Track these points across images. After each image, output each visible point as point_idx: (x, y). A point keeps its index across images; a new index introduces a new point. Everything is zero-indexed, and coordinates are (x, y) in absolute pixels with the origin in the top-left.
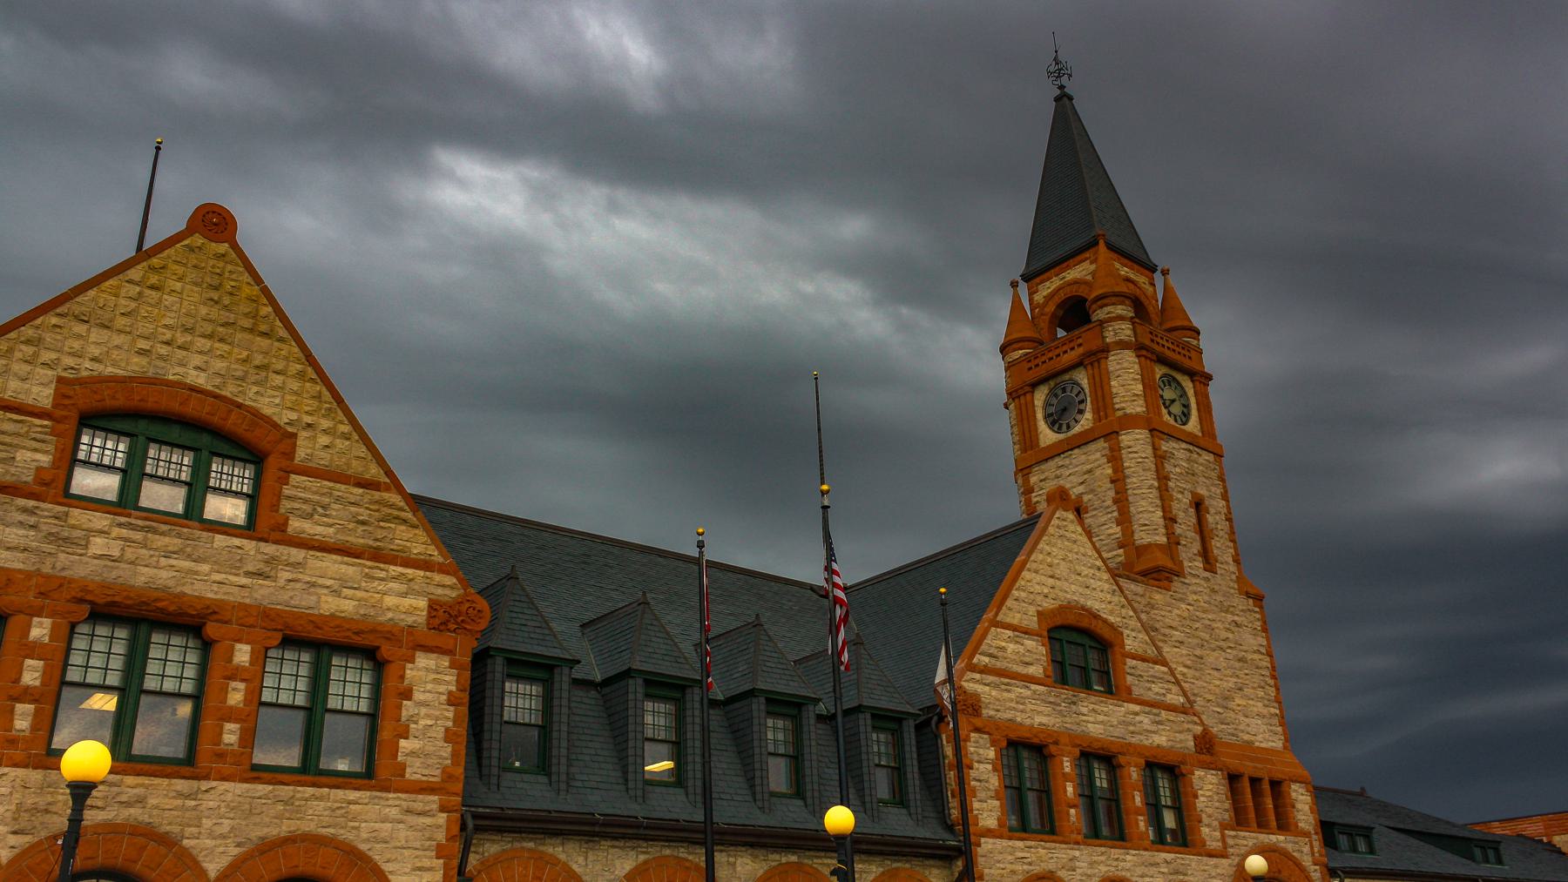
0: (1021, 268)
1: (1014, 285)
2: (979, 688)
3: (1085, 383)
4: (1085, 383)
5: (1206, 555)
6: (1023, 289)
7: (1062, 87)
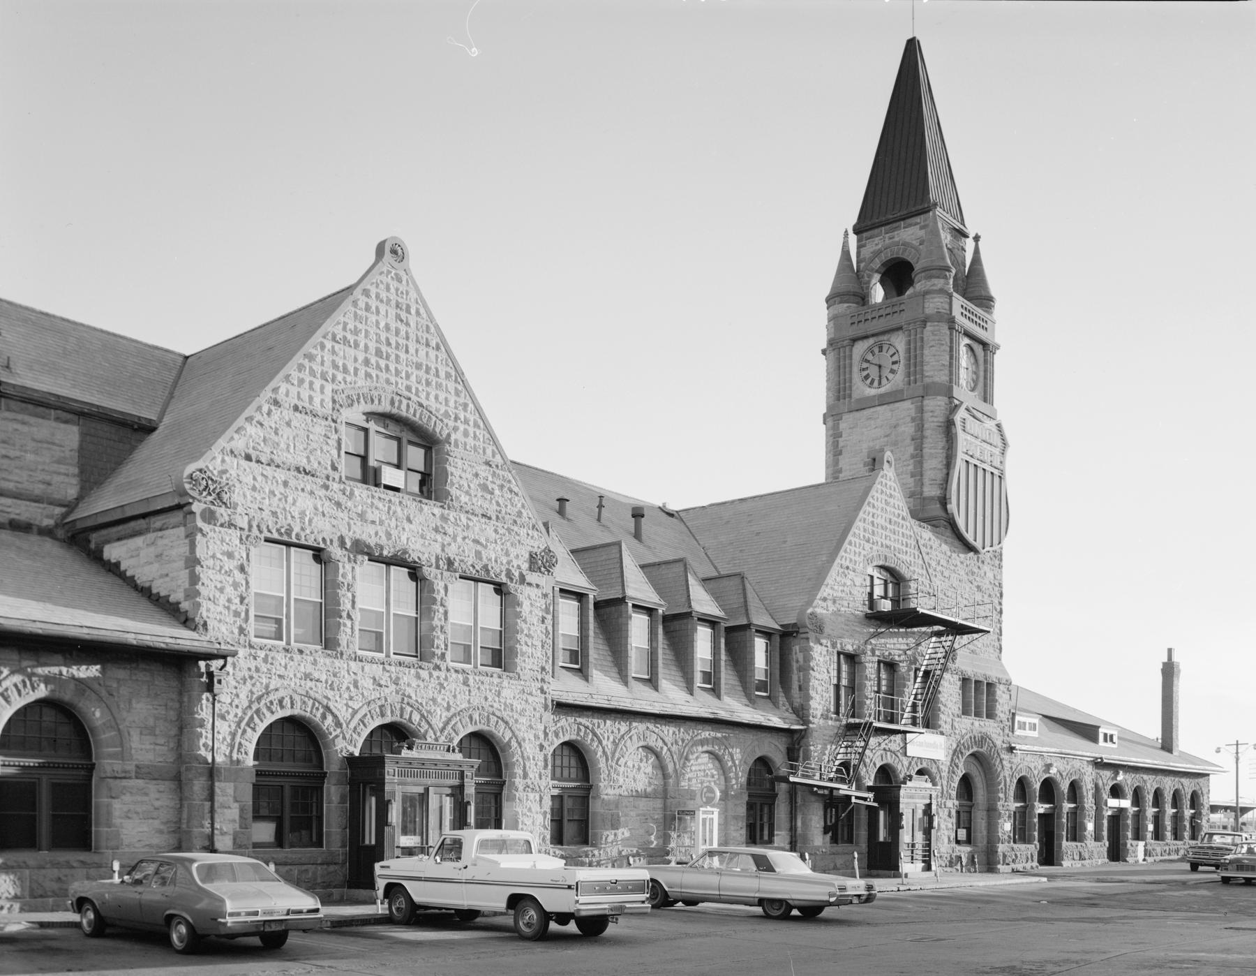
6: (853, 239)
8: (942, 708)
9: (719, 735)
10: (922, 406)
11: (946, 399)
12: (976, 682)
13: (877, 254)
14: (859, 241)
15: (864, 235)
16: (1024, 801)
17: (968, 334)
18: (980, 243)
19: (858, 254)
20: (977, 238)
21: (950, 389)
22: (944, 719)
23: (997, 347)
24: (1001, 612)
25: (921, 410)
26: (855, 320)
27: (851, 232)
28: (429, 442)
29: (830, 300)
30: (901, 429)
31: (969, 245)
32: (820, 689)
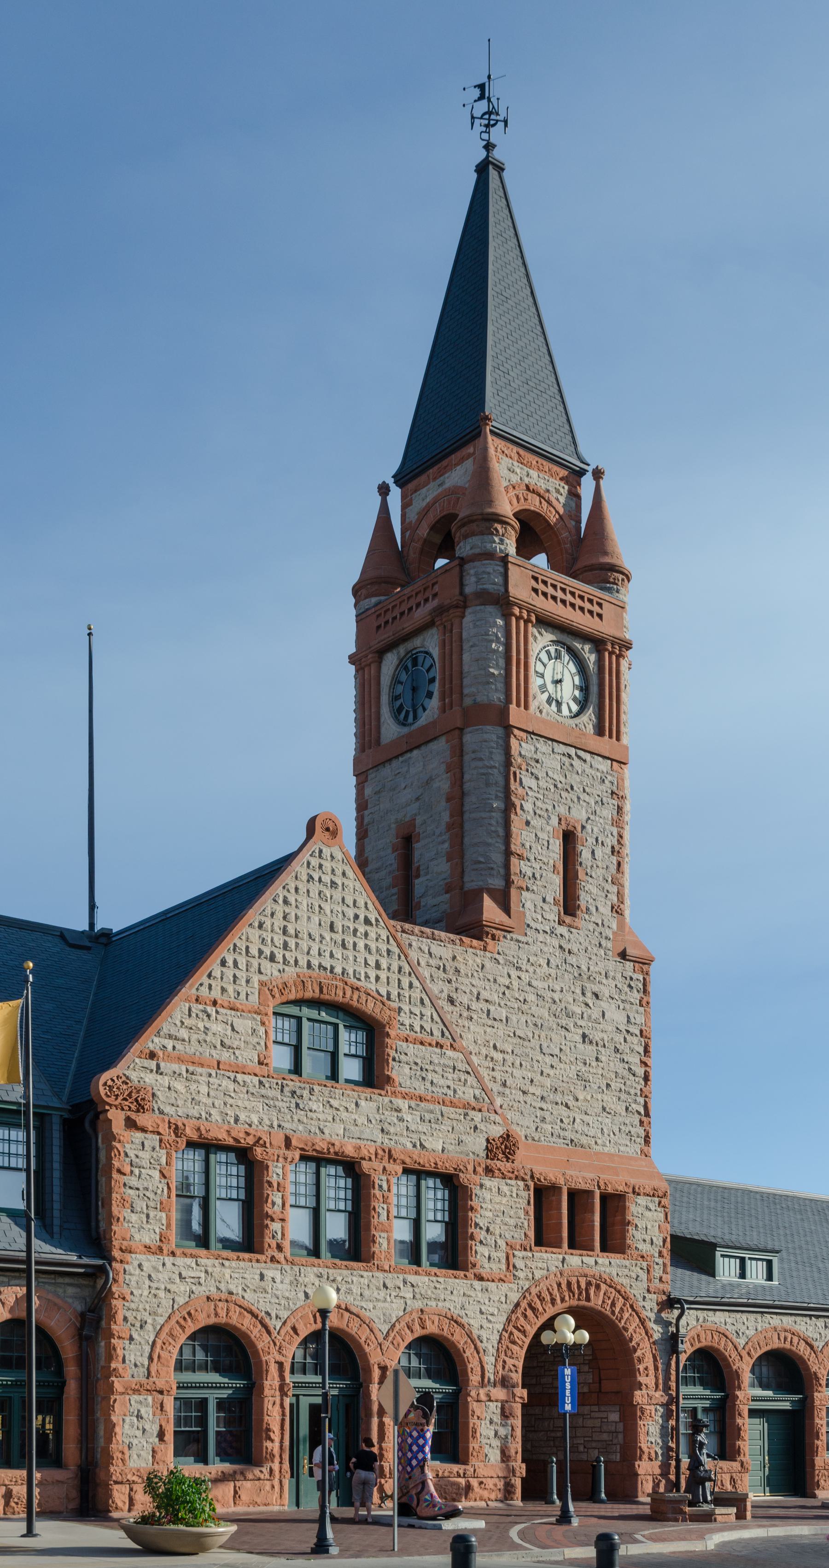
0: (394, 462)
1: (384, 490)
2: (150, 1079)
3: (435, 652)
4: (435, 652)
5: (570, 905)
6: (395, 493)
7: (489, 146)
8: (481, 1235)
9: (85, 1282)
10: (462, 744)
11: (500, 731)
12: (573, 1194)
13: (424, 513)
14: (403, 497)
15: (411, 486)
16: (722, 1389)
17: (545, 622)
18: (602, 483)
19: (403, 516)
20: (598, 474)
21: (504, 713)
22: (485, 1253)
23: (626, 645)
24: (646, 1078)
25: (459, 751)
26: (382, 621)
27: (390, 482)
28: (644, 963)
29: (357, 591)
30: (436, 784)
31: (587, 486)
32: (140, 1205)
